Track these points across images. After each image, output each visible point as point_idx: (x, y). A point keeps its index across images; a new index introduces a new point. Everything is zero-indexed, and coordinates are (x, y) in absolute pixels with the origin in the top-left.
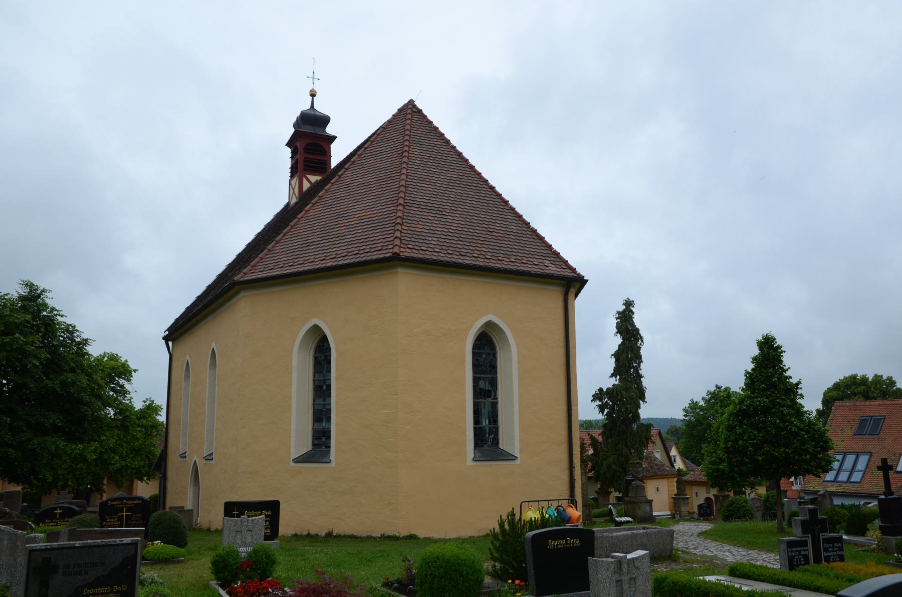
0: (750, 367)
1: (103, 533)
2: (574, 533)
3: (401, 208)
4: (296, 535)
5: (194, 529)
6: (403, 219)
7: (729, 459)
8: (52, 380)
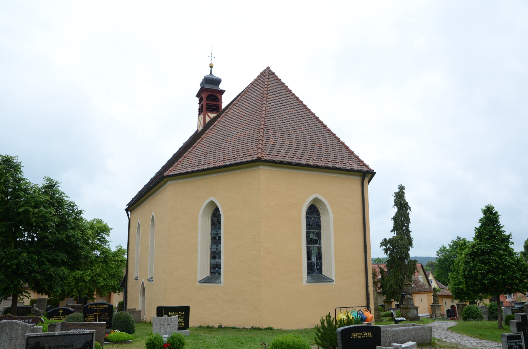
0: (478, 225)
1: (84, 325)
2: (368, 329)
3: (262, 130)
4: (200, 327)
5: (142, 322)
6: (263, 137)
7: (466, 282)
8: (61, 234)
